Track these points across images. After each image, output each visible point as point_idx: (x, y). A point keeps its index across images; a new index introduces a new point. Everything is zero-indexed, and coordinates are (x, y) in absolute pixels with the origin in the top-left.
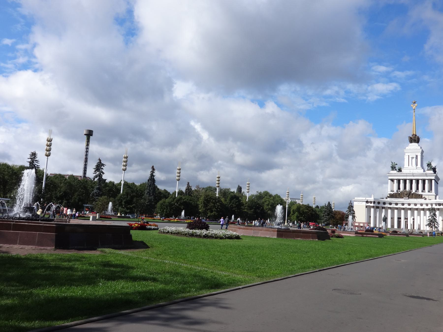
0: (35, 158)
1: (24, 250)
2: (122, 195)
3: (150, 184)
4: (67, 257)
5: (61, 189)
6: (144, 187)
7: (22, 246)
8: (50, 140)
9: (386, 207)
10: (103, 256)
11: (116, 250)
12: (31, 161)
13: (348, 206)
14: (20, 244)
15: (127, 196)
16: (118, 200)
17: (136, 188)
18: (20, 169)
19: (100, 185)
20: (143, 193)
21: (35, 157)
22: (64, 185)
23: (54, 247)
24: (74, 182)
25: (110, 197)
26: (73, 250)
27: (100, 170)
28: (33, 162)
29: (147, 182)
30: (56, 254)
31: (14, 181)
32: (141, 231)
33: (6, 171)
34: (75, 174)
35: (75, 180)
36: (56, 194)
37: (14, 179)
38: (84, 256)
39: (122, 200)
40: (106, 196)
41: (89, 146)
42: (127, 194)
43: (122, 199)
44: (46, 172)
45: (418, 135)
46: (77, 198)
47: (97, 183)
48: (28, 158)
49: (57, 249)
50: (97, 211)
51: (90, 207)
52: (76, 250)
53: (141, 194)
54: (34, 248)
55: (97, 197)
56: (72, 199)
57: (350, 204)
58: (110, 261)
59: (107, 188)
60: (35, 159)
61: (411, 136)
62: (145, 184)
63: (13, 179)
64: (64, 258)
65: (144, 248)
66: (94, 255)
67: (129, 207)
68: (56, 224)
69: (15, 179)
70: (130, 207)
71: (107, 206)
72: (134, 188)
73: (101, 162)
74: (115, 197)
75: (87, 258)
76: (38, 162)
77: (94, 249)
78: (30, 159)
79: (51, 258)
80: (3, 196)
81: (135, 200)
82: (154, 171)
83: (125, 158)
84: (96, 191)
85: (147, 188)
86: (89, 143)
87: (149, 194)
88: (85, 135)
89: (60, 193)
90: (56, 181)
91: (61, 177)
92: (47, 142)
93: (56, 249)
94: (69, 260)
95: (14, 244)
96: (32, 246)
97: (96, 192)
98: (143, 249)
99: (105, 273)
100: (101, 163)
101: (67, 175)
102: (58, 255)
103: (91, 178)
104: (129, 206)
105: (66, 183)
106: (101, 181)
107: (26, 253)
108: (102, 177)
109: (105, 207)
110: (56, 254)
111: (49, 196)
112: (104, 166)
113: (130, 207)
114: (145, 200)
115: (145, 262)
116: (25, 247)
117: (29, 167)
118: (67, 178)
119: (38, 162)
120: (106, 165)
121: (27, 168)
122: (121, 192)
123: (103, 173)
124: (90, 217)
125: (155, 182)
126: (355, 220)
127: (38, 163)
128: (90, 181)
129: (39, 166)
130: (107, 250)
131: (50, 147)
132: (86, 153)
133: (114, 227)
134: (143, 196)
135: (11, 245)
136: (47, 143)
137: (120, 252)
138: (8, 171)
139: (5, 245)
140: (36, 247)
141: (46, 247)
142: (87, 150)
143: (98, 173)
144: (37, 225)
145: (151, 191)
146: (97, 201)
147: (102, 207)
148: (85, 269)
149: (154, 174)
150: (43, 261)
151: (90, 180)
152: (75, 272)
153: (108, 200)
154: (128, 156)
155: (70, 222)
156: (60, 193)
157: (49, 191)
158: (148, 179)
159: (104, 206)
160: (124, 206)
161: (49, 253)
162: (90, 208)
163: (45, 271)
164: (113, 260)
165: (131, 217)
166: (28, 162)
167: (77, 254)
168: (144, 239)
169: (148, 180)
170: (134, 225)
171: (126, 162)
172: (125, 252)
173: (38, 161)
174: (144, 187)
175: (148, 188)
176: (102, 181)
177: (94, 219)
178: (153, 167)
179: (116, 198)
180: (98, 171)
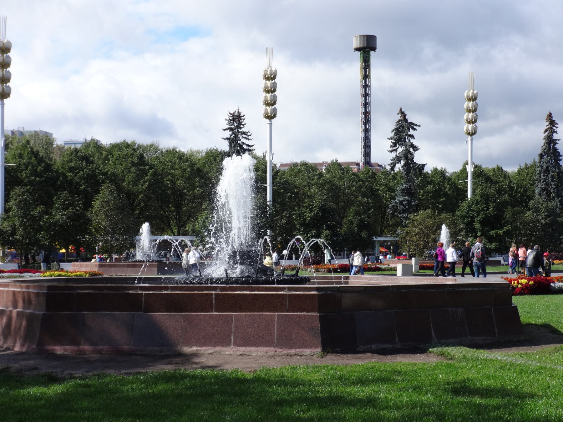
0: (241, 128)
1: (250, 359)
2: (473, 203)
3: (547, 167)
4: (355, 372)
5: (312, 202)
6: (530, 175)
7: (242, 350)
8: (271, 77)
10: (448, 366)
11: (478, 351)
12: (231, 136)
14: (237, 344)
15: (487, 204)
16: (463, 218)
17: (507, 181)
18: (207, 158)
19: (409, 180)
20: (529, 193)
21: (240, 124)
22: (320, 191)
23: (319, 350)
24: (343, 179)
25: (440, 211)
26: (368, 354)
27: (405, 141)
28: (236, 137)
29: (537, 160)
30: (327, 367)
31: (198, 191)
32: (537, 297)
33: (177, 169)
34: (342, 159)
35: (343, 174)
36: (301, 215)
37: (198, 187)
38: (399, 368)
39: (473, 217)
40: (429, 211)
41: (369, 79)
42: (486, 198)
43: (473, 215)
44: (271, 161)
46: (355, 222)
47: (401, 177)
48: (225, 130)
49: (328, 352)
50: (409, 251)
51: (391, 241)
52: (376, 355)
53: (522, 195)
54: (273, 353)
55: (405, 215)
56: (342, 225)
58: (468, 379)
59: (430, 188)
62: (531, 166)
63: (195, 187)
64: (349, 377)
65: (557, 343)
66: (424, 364)
67: (494, 235)
68: (317, 289)
69: (201, 187)
70: (498, 236)
71: (434, 236)
72: (501, 182)
73: (407, 117)
74: (453, 212)
75: (405, 373)
76: (249, 137)
77: (423, 351)
78: (228, 130)
79: (316, 378)
80: (179, 232)
81: (508, 213)
82: (554, 128)
83: (469, 99)
84: (400, 199)
85: (540, 177)
86: (369, 72)
87: (546, 193)
88: (357, 49)
89: (311, 211)
90: (299, 181)
91: (308, 171)
92: (264, 81)
93: (325, 353)
94: (363, 381)
95: (223, 346)
96: (265, 349)
97: (401, 202)
98: (552, 345)
99: (459, 411)
100: (405, 120)
101: (321, 164)
102: (332, 369)
103: (383, 166)
104: (493, 232)
105: (322, 186)
106: (412, 171)
107: (255, 366)
108: (413, 158)
109: (430, 240)
110: (327, 367)
111: (284, 221)
112: (415, 129)
113: (496, 233)
114: (537, 210)
116: (250, 351)
117: (229, 153)
118: (324, 171)
119: (249, 137)
120: (419, 126)
121: (229, 155)
122: (469, 196)
123: (415, 148)
124: (395, 269)
125: (561, 158)
127: (249, 139)
128: (382, 172)
129: (253, 146)
130: (457, 351)
131: (275, 95)
132: (365, 100)
133: (466, 289)
134: (531, 203)
135: (218, 348)
136: (266, 83)
137: (490, 354)
138: (181, 168)
139: (204, 348)
140: (276, 351)
141: (301, 350)
142: (365, 90)
143: (400, 150)
144: (273, 294)
145: (551, 185)
146: (406, 226)
147: (421, 239)
148: (407, 402)
149: (555, 136)
150: (299, 384)
151: (382, 170)
152: (383, 409)
153: (435, 219)
154: (477, 93)
155: (349, 283)
156: (310, 213)
157: (284, 210)
158: (540, 151)
159: (427, 237)
160: (479, 234)
161: (311, 364)
162: (390, 246)
163: (309, 410)
164: (477, 376)
165: (502, 262)
166: (225, 139)
167: (379, 365)
168: (551, 318)
169: (541, 156)
170: (516, 282)
171: (473, 111)
172: (505, 356)
173: (249, 134)
174: (530, 175)
175: (542, 177)
177: (407, 271)
178: (550, 116)
179: (458, 214)
180: (401, 145)
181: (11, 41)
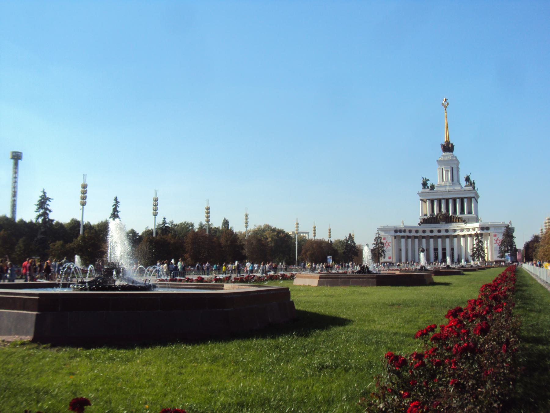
9: (427, 236)
13: (375, 237)
45: (451, 142)
57: (378, 235)
60: (476, 258)
82: (118, 205)
100: (45, 196)
112: (50, 201)
120: (53, 199)
123: (50, 211)
126: (385, 255)
149: (118, 209)
176: (47, 223)
180: (42, 209)
181: (515, 230)
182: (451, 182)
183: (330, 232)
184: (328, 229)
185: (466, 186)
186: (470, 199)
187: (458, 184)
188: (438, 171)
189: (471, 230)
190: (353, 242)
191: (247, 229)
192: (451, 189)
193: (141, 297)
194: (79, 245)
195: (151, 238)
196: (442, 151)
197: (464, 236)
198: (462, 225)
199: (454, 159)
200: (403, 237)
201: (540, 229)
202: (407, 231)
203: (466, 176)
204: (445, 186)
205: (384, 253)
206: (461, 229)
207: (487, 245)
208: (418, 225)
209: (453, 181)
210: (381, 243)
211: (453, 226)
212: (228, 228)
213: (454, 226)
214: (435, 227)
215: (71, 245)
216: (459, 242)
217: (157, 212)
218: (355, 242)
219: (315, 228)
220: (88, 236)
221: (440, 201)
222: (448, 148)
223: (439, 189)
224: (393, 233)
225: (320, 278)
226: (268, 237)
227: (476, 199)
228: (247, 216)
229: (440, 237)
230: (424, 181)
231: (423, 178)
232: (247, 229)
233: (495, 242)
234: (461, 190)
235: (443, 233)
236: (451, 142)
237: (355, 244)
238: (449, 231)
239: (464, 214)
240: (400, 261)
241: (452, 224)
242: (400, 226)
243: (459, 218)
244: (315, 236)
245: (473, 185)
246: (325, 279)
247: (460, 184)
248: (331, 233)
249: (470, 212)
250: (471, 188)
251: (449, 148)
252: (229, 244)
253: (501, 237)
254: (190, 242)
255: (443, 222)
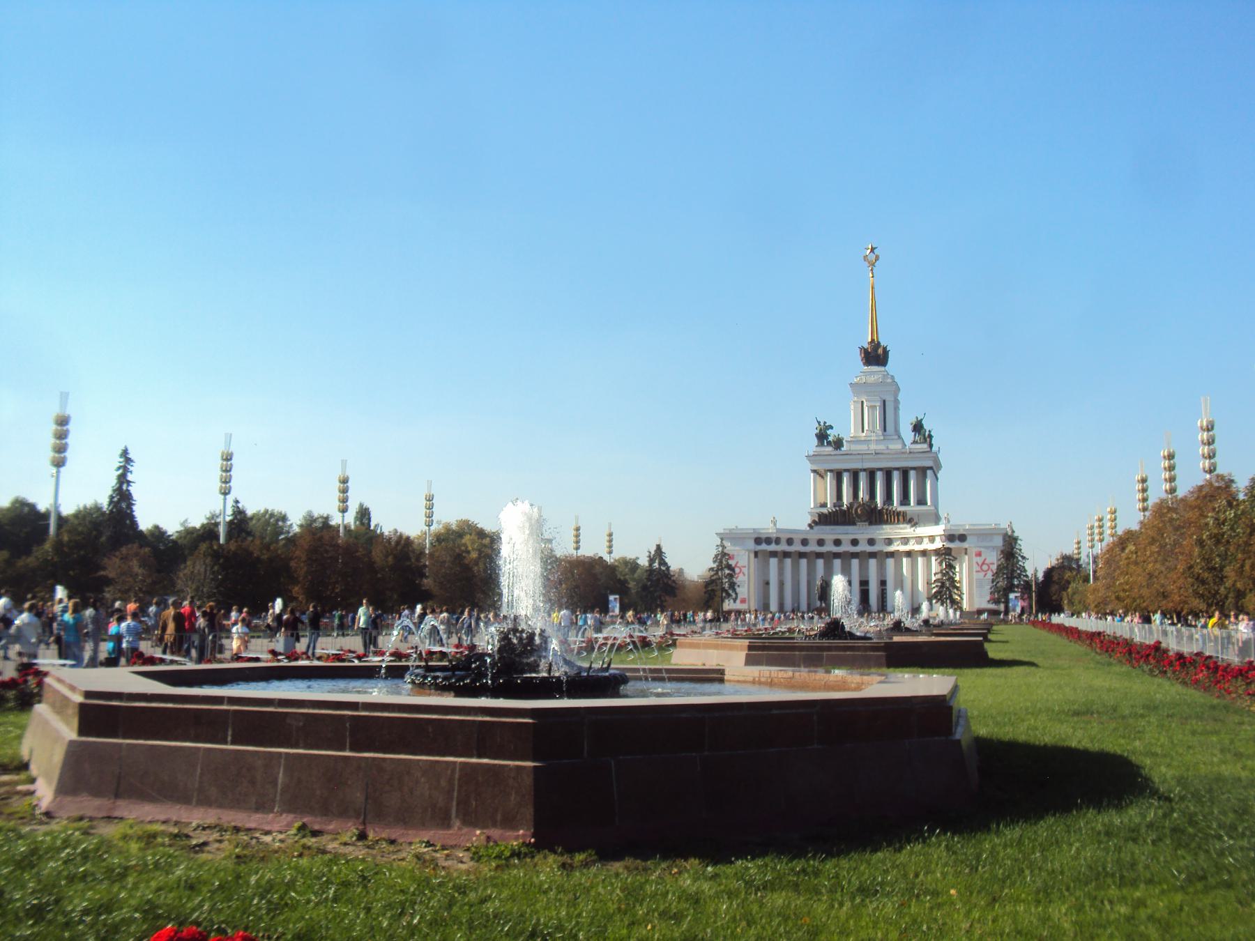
9: (828, 552)
61: (866, 346)
82: (129, 467)
115: (896, 882)
126: (736, 594)
149: (130, 477)
182: (880, 433)
183: (610, 541)
184: (607, 532)
185: (915, 442)
186: (922, 472)
187: (896, 437)
188: (852, 407)
189: (926, 540)
190: (665, 564)
191: (429, 529)
192: (881, 447)
193: (775, 712)
194: (46, 560)
195: (215, 547)
196: (862, 363)
197: (909, 554)
198: (904, 529)
199: (889, 380)
200: (774, 554)
201: (1075, 541)
202: (783, 541)
203: (914, 421)
204: (866, 442)
205: (734, 590)
206: (900, 536)
207: (963, 573)
208: (808, 528)
209: (885, 430)
210: (729, 567)
211: (885, 531)
212: (369, 525)
213: (889, 531)
214: (845, 533)
215: (31, 561)
216: (899, 566)
217: (230, 487)
218: (669, 564)
219: (578, 529)
220: (70, 541)
221: (855, 475)
222: (875, 356)
223: (855, 447)
224: (751, 545)
225: (750, 648)
226: (470, 548)
227: (934, 472)
228: (430, 499)
229: (855, 555)
230: (821, 430)
231: (819, 423)
232: (429, 529)
233: (979, 569)
234: (903, 450)
235: (863, 547)
236: (882, 344)
237: (668, 568)
238: (877, 541)
239: (909, 504)
240: (766, 607)
241: (884, 526)
242: (767, 528)
243: (898, 514)
244: (577, 548)
245: (928, 440)
246: (763, 651)
247: (900, 437)
248: (581, 537)
249: (921, 501)
250: (925, 446)
251: (878, 356)
252: (390, 563)
253: (993, 559)
254: (304, 558)
255: (865, 521)
